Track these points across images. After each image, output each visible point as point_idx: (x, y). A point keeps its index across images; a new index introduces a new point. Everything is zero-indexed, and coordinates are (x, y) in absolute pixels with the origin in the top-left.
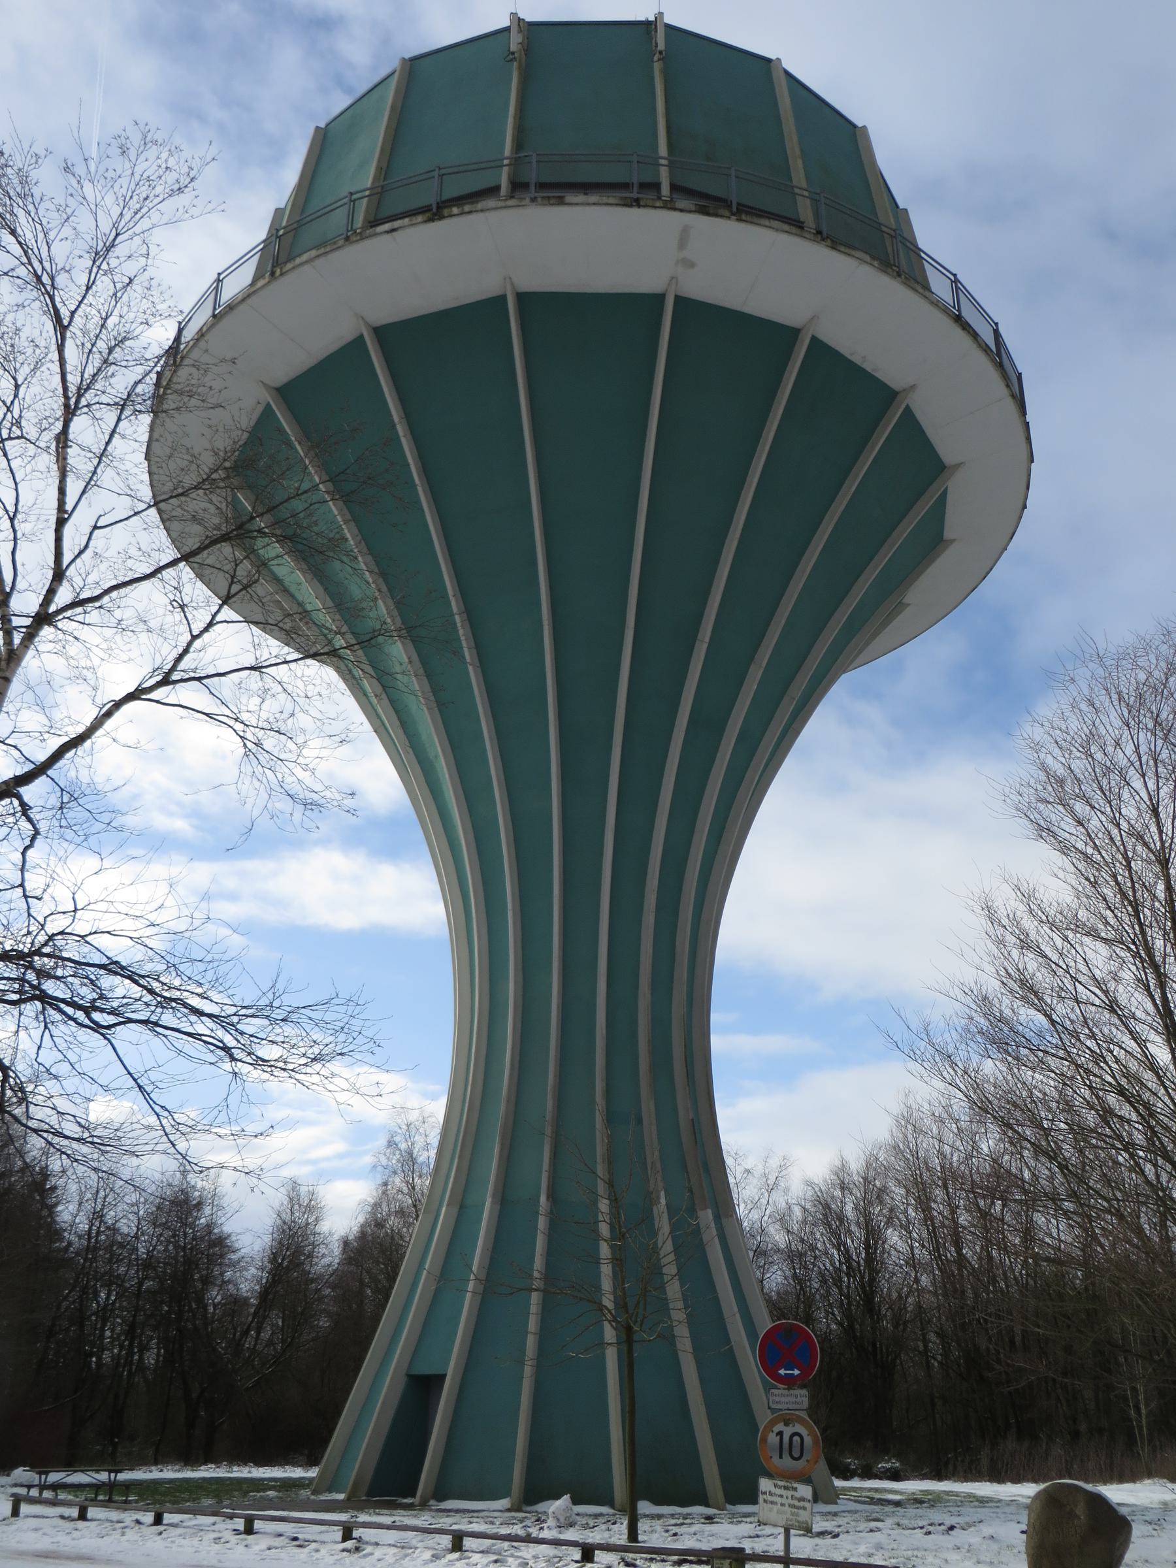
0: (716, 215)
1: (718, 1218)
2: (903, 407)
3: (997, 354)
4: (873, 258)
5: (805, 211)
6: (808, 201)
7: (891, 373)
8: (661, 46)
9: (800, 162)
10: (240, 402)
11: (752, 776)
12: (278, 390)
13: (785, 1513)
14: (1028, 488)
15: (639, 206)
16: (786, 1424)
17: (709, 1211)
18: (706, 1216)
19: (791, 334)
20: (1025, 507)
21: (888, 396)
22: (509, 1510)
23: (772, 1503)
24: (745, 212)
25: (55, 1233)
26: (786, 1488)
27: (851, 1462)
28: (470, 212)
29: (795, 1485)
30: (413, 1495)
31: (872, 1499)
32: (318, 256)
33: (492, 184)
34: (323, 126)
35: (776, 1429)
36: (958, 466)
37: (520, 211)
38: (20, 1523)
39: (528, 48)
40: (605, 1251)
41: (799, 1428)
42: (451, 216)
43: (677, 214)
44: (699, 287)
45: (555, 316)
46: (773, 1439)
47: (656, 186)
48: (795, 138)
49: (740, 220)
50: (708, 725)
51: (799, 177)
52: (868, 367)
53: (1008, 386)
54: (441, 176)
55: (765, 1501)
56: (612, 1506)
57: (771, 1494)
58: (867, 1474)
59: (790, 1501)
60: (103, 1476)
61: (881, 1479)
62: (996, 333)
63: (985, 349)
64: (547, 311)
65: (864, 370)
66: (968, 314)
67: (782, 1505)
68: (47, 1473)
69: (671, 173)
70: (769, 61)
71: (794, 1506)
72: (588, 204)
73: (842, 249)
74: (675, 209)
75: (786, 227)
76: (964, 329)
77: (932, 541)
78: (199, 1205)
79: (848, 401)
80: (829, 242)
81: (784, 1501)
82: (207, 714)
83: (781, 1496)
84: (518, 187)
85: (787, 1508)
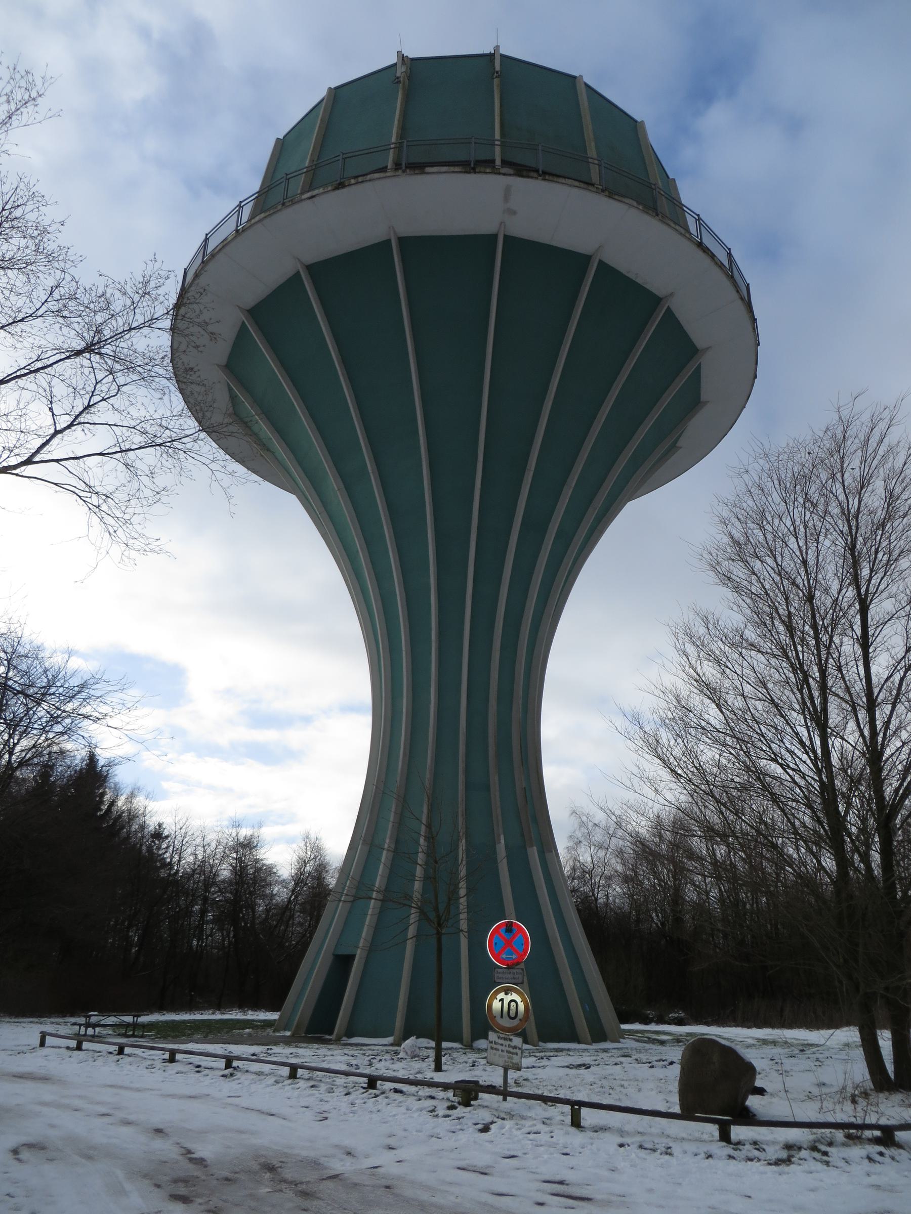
0: (528, 177)
1: (542, 854)
2: (665, 308)
3: (730, 271)
5: (595, 178)
6: (597, 167)
7: (656, 284)
8: (498, 68)
9: (593, 144)
10: (227, 322)
11: (568, 561)
12: (248, 311)
13: (503, 1056)
14: (757, 364)
15: (475, 172)
16: (506, 994)
17: (535, 848)
18: (533, 853)
19: (585, 259)
20: (755, 377)
21: (655, 301)
22: (392, 1045)
23: (496, 1049)
24: (546, 175)
26: (505, 1039)
27: (651, 1013)
28: (362, 182)
30: (331, 1033)
31: (649, 1038)
32: (265, 217)
33: (488, 158)
38: (45, 1051)
39: (410, 76)
40: (419, 872)
42: (350, 185)
44: (521, 228)
47: (493, 161)
48: (590, 127)
49: (544, 179)
50: (535, 527)
51: (592, 152)
53: (738, 291)
54: (344, 159)
56: (462, 1043)
57: (495, 1043)
58: (661, 1021)
59: (507, 1048)
60: (129, 1019)
61: (669, 1024)
62: (730, 255)
63: (721, 265)
64: (417, 248)
66: (708, 241)
67: (502, 1051)
69: (502, 152)
70: (575, 77)
72: (441, 173)
73: (616, 197)
76: (704, 252)
77: (692, 401)
79: (626, 303)
80: (607, 193)
81: (503, 1048)
82: (56, 484)
83: (502, 1045)
84: (397, 166)
85: (505, 1054)
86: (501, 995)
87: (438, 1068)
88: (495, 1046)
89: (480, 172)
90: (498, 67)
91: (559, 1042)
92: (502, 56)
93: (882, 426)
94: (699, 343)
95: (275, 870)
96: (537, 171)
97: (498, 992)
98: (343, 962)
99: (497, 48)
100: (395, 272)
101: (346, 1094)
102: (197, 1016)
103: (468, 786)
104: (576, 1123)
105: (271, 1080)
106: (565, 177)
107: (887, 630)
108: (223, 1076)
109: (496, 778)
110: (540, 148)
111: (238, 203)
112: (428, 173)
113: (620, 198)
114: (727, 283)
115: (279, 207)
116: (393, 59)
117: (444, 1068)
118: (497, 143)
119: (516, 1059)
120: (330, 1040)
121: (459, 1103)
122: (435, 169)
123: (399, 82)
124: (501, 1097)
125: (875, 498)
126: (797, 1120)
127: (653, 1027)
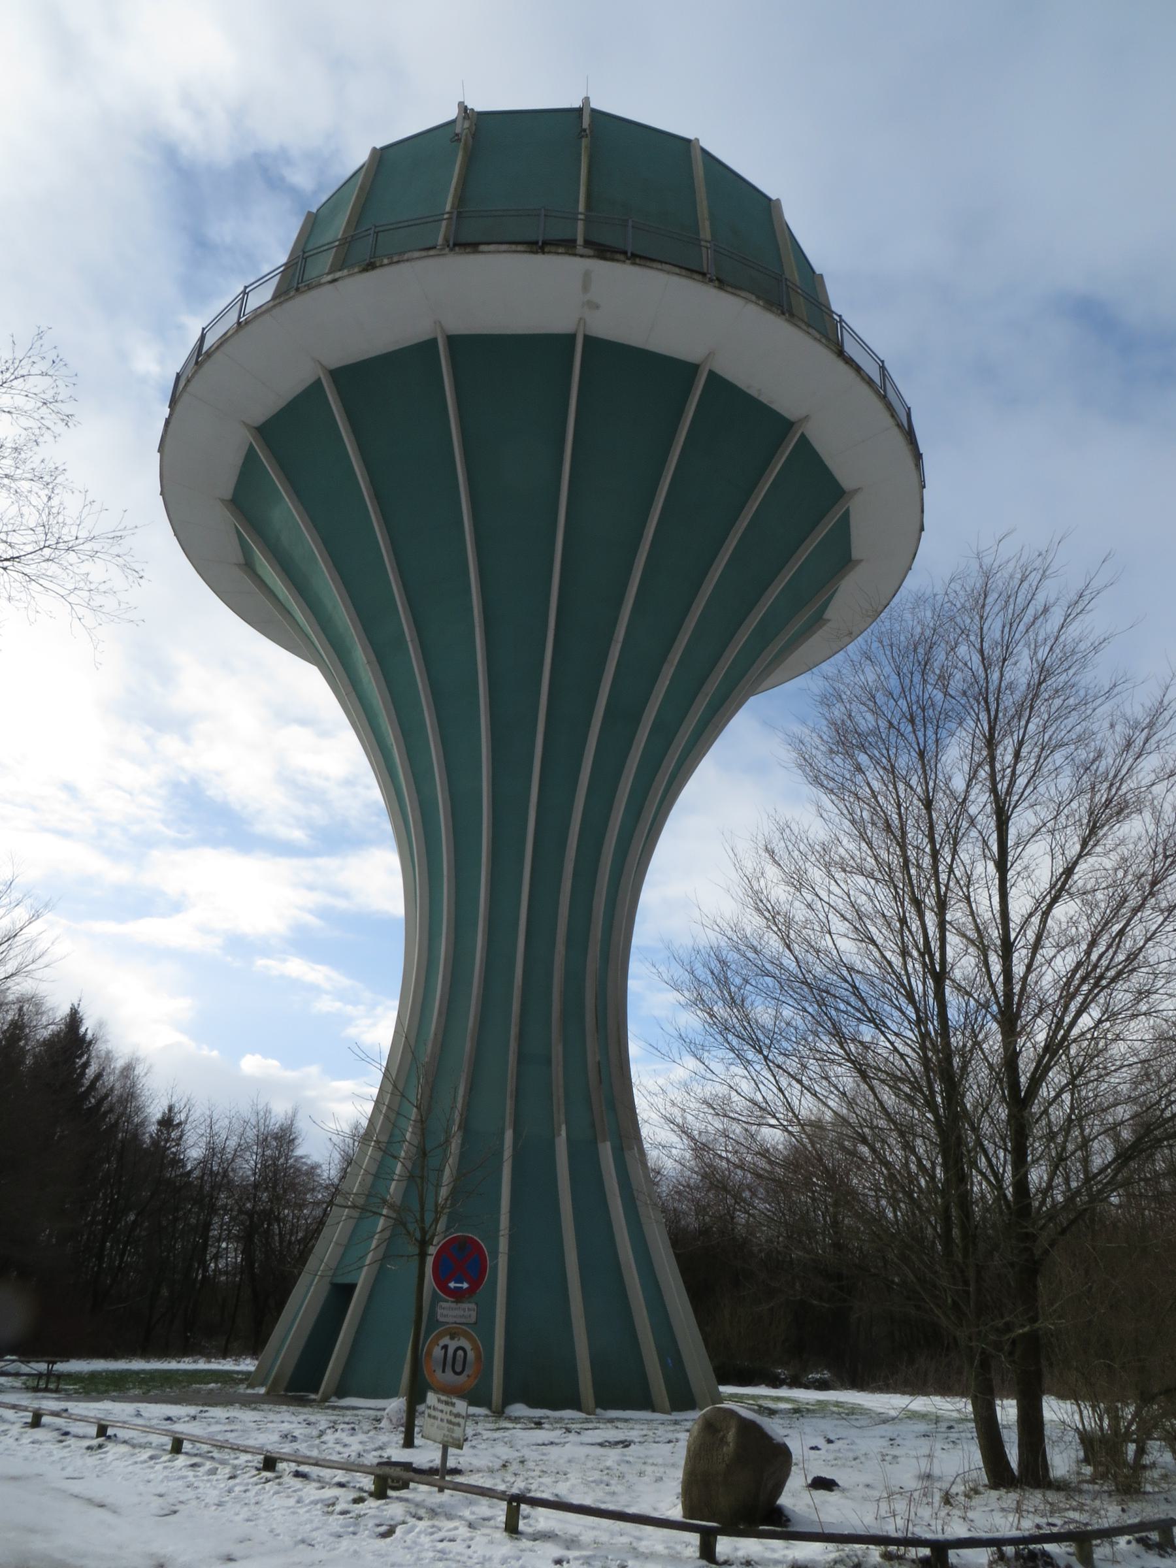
0: (613, 260)
2: (798, 435)
4: (758, 297)
9: (707, 223)
13: (442, 1428)
15: (544, 253)
16: (452, 1338)
17: (608, 1144)
18: (606, 1150)
19: (692, 369)
20: (922, 529)
23: (435, 1418)
24: (636, 258)
25: (177, 1162)
26: (447, 1403)
28: (398, 262)
29: (454, 1400)
30: (316, 1391)
34: (314, 211)
35: (442, 1342)
36: (856, 491)
37: (441, 260)
41: (464, 1342)
42: (382, 266)
43: (577, 260)
44: (605, 327)
45: (486, 358)
46: (438, 1352)
47: (575, 241)
48: (705, 203)
49: (634, 264)
50: (624, 717)
51: (706, 233)
52: (764, 399)
53: (893, 416)
55: (429, 1416)
58: (795, 1383)
60: (42, 1367)
62: (883, 368)
63: (869, 382)
65: (760, 402)
67: (442, 1420)
68: (54, 1363)
70: (688, 141)
71: (449, 1422)
72: (499, 252)
73: (729, 289)
74: (575, 255)
75: (677, 270)
76: (847, 363)
77: (839, 557)
78: (284, 1138)
79: (744, 428)
85: (445, 1425)
86: (445, 1340)
87: (409, 1443)
88: (433, 1413)
89: (549, 252)
90: (586, 122)
91: (624, 1409)
92: (594, 111)
93: (1034, 578)
94: (846, 482)
95: (319, 1171)
96: (625, 253)
97: (440, 1336)
98: (342, 1292)
99: (587, 100)
100: (443, 382)
101: (231, 1478)
102: (173, 1365)
103: (521, 1059)
104: (512, 1528)
105: (145, 1454)
106: (661, 262)
107: (1032, 849)
108: (89, 1448)
109: (560, 1048)
110: (630, 224)
111: (242, 289)
112: (483, 252)
113: (733, 290)
114: (879, 405)
115: (292, 293)
116: (451, 113)
117: (417, 1442)
118: (581, 217)
119: (458, 1433)
120: (314, 1400)
121: (371, 1494)
122: (492, 247)
123: (459, 140)
124: (436, 1489)
125: (1021, 671)
126: (826, 1531)
127: (784, 1392)
